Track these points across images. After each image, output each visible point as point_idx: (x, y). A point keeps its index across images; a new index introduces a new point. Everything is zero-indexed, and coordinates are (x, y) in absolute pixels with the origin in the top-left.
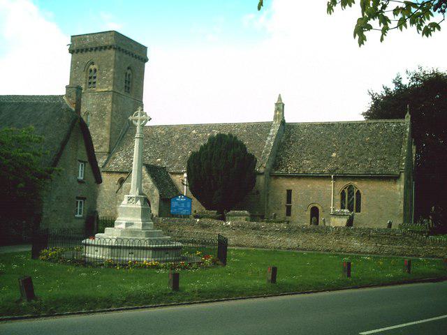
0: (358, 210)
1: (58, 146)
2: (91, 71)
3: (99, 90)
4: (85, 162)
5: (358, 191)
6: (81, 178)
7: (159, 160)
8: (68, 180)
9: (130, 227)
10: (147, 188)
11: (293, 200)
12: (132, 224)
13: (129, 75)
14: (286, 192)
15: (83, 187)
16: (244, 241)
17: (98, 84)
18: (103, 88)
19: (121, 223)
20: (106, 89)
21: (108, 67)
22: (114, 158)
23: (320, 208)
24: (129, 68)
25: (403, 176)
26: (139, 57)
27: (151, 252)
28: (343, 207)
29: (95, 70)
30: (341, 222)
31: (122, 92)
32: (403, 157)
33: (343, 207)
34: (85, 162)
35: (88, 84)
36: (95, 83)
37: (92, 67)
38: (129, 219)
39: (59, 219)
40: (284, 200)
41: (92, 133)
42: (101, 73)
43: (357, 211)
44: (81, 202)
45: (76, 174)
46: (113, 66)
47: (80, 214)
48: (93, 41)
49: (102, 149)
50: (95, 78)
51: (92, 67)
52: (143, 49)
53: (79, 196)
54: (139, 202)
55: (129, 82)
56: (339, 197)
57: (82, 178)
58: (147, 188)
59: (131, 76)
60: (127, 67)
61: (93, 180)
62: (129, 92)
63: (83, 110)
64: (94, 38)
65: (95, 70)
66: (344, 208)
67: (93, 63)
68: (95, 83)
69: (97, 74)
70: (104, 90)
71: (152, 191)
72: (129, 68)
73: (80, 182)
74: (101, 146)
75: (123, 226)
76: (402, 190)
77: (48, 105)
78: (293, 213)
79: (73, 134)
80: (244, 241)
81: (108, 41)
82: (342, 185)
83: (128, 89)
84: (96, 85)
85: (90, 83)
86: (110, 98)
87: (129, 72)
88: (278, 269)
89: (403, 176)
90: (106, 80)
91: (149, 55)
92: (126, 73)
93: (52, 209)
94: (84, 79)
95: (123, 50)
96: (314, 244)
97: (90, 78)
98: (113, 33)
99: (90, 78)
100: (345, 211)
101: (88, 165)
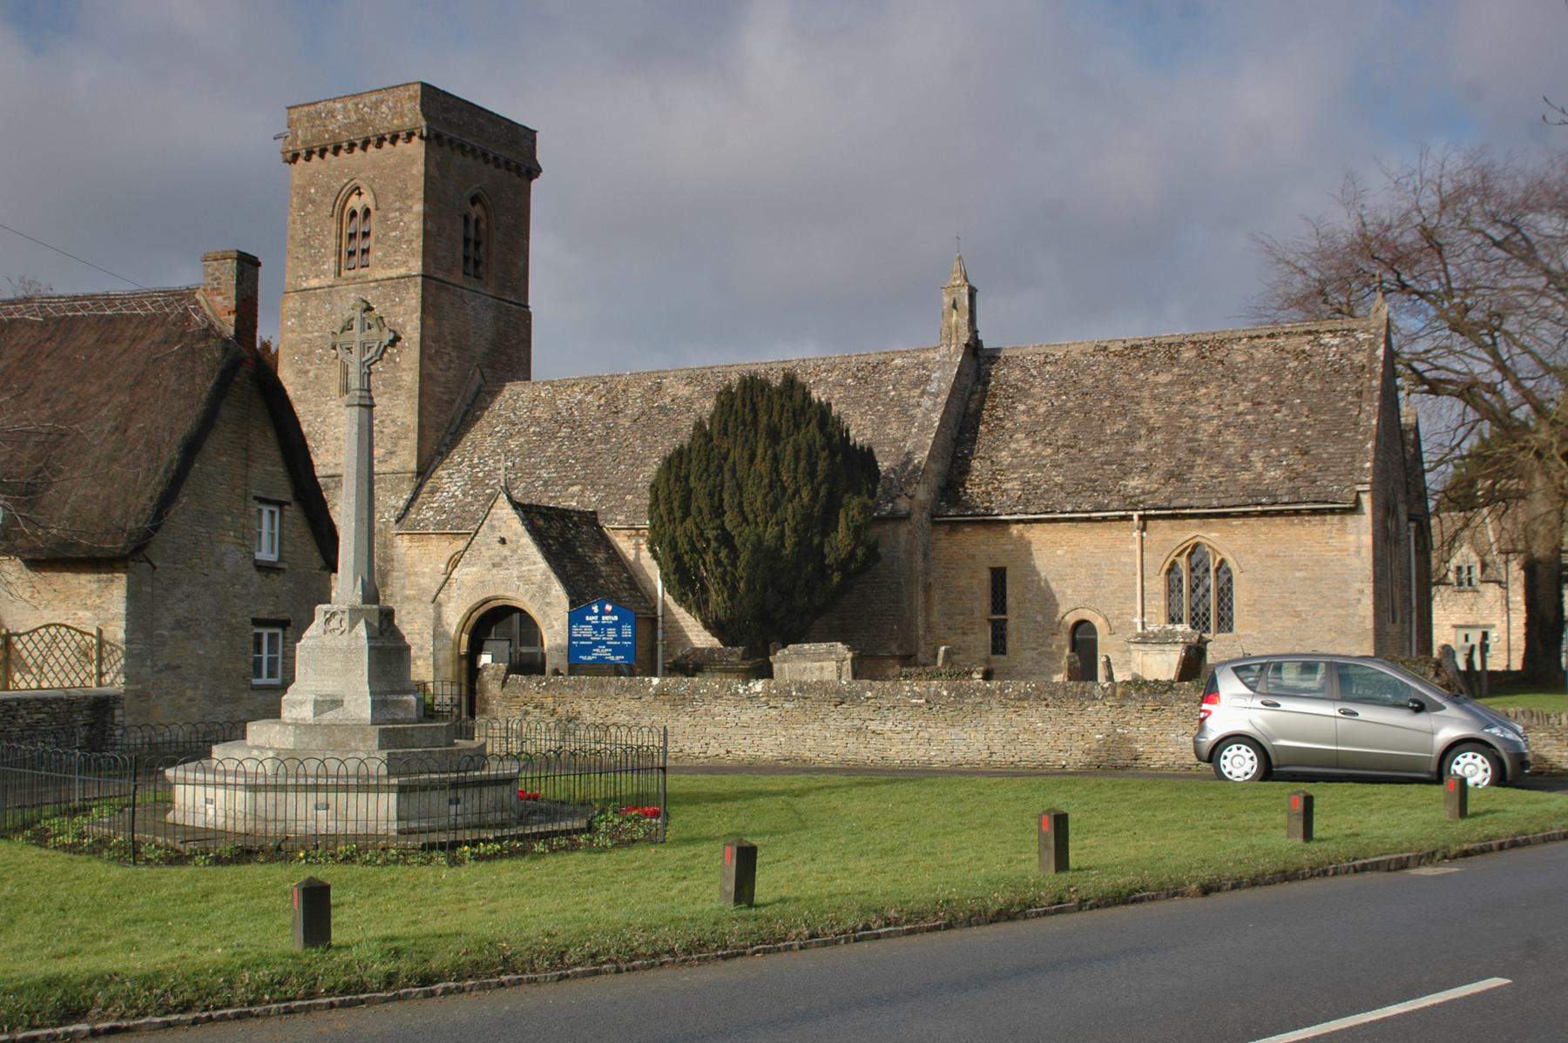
0: (1225, 623)
1: (171, 453)
2: (354, 214)
3: (380, 274)
4: (281, 504)
5: (1222, 561)
6: (266, 554)
7: (576, 489)
8: (219, 565)
9: (328, 717)
10: (528, 582)
11: (1010, 601)
12: (336, 703)
13: (477, 222)
14: (986, 575)
15: (277, 583)
16: (810, 743)
17: (376, 254)
18: (390, 266)
19: (302, 703)
20: (403, 271)
21: (403, 195)
22: (433, 492)
23: (1098, 622)
24: (475, 200)
25: (1366, 501)
26: (507, 163)
27: (393, 796)
28: (1173, 619)
29: (367, 212)
30: (1162, 664)
31: (457, 277)
32: (1364, 442)
33: (1173, 619)
34: (281, 504)
35: (344, 255)
36: (365, 251)
37: (355, 203)
38: (330, 687)
39: (189, 693)
40: (982, 605)
41: (299, 409)
42: (385, 219)
43: (1220, 630)
44: (272, 637)
45: (249, 538)
46: (421, 194)
47: (271, 674)
48: (354, 117)
49: (395, 464)
50: (366, 235)
51: (355, 203)
52: (522, 138)
53: (263, 615)
54: (361, 630)
55: (477, 244)
56: (1157, 585)
57: (274, 557)
58: (528, 582)
59: (483, 226)
60: (467, 194)
61: (316, 559)
62: (478, 277)
63: (263, 333)
64: (357, 110)
65: (367, 212)
66: (1180, 621)
67: (357, 190)
68: (365, 251)
69: (374, 224)
70: (393, 273)
71: (546, 591)
72: (475, 200)
73: (264, 568)
74: (392, 453)
75: (307, 713)
76: (1367, 554)
77: (151, 319)
78: (1012, 642)
79: (225, 412)
80: (810, 743)
81: (402, 115)
82: (1171, 537)
83: (473, 265)
84: (372, 258)
85: (352, 254)
86: (413, 297)
87: (476, 211)
88: (1072, 818)
89: (1366, 501)
90: (399, 240)
91: (541, 157)
92: (466, 219)
93: (160, 664)
94: (332, 242)
95: (451, 141)
96: (1041, 746)
97: (352, 236)
98: (418, 87)
99: (352, 236)
100: (1179, 628)
101: (292, 511)
